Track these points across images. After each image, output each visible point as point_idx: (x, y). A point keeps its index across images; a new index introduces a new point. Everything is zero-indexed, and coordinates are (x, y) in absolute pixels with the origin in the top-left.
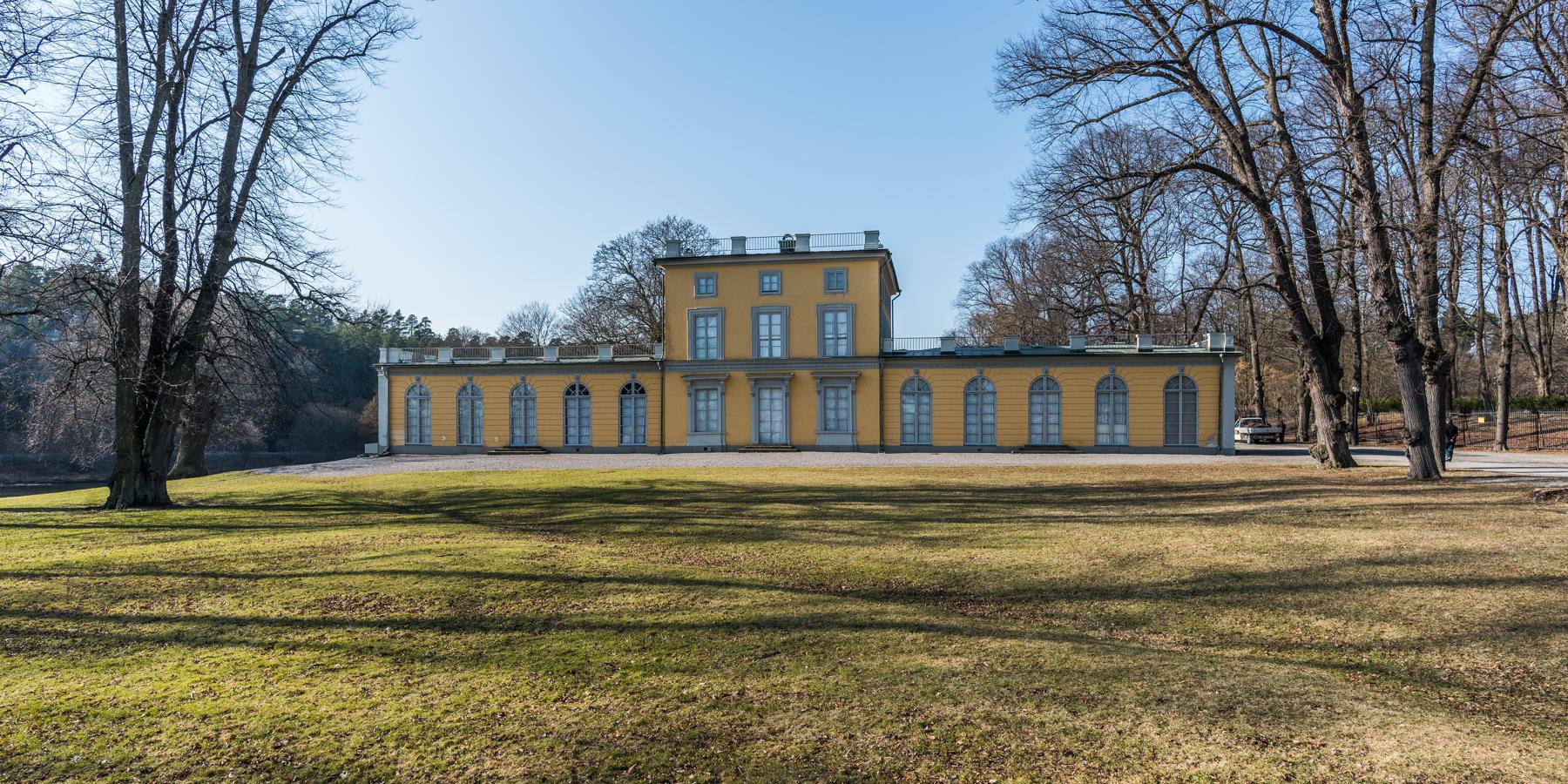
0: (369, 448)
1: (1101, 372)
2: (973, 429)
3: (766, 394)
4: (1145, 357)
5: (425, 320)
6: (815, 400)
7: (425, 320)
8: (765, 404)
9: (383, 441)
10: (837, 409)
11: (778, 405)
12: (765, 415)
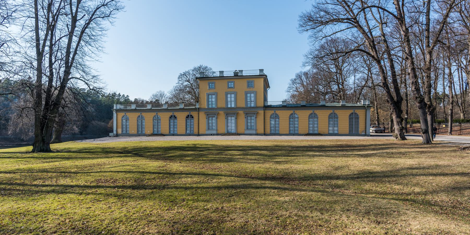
0: (111, 134)
1: (330, 111)
2: (292, 129)
3: (230, 118)
4: (343, 107)
5: (128, 96)
6: (244, 120)
7: (128, 96)
8: (229, 121)
9: (115, 132)
10: (251, 122)
11: (233, 121)
12: (229, 124)
